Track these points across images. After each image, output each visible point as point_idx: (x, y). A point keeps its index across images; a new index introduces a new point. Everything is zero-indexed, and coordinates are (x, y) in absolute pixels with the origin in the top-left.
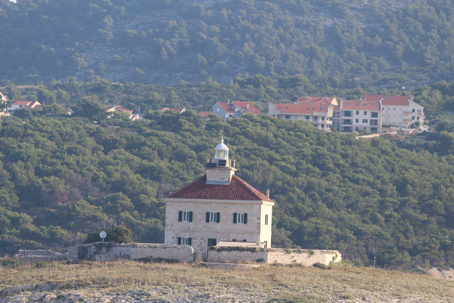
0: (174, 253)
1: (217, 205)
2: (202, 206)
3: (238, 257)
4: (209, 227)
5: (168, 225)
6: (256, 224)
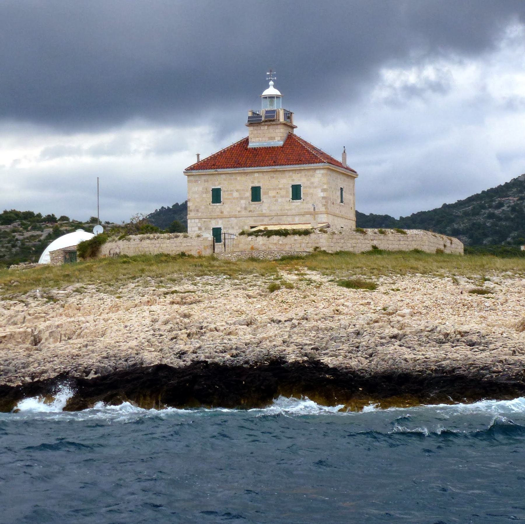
0: (184, 245)
1: (261, 175)
2: (238, 178)
3: (281, 245)
4: (252, 209)
5: (191, 211)
6: (321, 199)
